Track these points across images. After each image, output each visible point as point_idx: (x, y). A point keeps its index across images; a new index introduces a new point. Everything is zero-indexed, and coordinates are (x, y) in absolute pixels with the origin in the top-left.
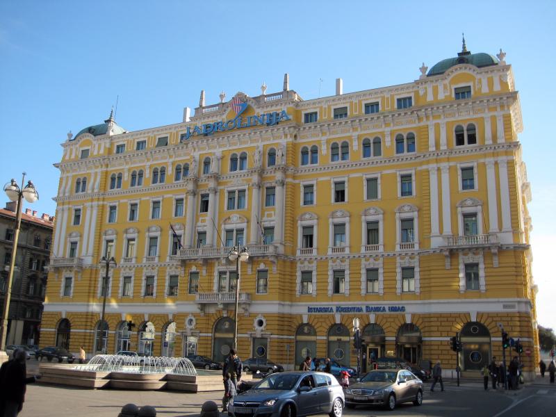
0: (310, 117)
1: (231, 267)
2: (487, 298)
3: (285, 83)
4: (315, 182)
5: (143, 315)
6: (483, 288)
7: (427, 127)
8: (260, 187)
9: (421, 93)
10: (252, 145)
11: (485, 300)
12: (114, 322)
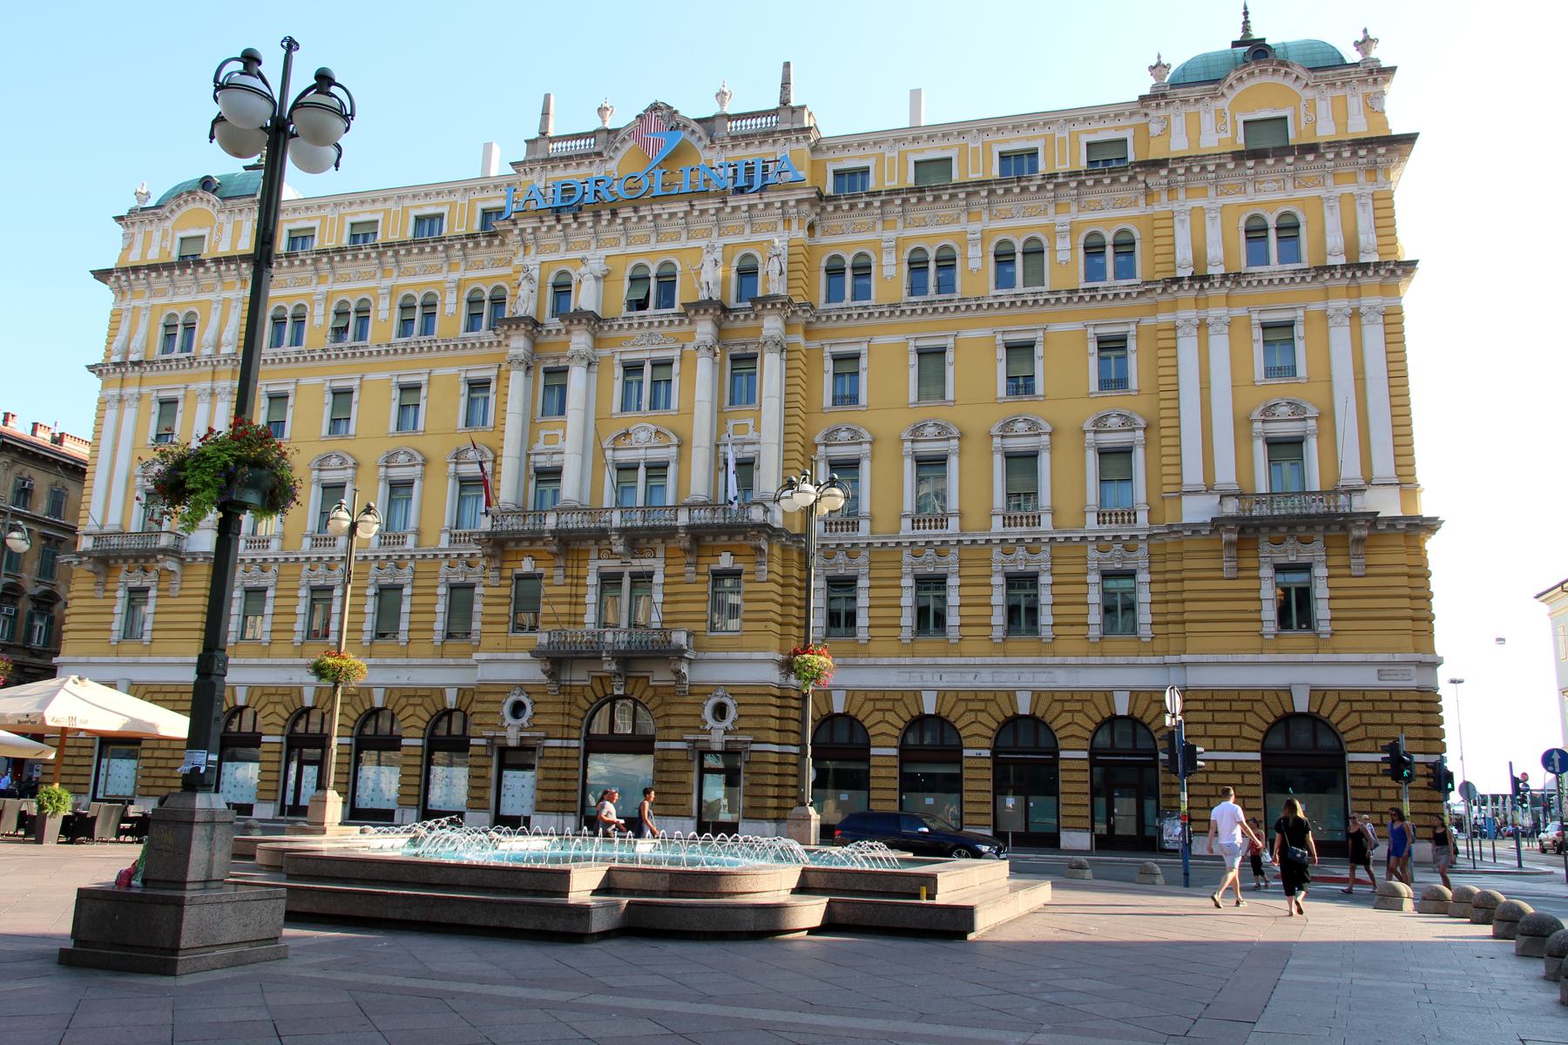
0: (851, 179)
1: (635, 562)
2: (1335, 651)
3: (546, 113)
4: (678, 352)
5: (442, 691)
6: (1145, 631)
7: (1172, 216)
8: (528, 368)
9: (1155, 128)
10: (693, 244)
11: (1334, 658)
12: (280, 709)
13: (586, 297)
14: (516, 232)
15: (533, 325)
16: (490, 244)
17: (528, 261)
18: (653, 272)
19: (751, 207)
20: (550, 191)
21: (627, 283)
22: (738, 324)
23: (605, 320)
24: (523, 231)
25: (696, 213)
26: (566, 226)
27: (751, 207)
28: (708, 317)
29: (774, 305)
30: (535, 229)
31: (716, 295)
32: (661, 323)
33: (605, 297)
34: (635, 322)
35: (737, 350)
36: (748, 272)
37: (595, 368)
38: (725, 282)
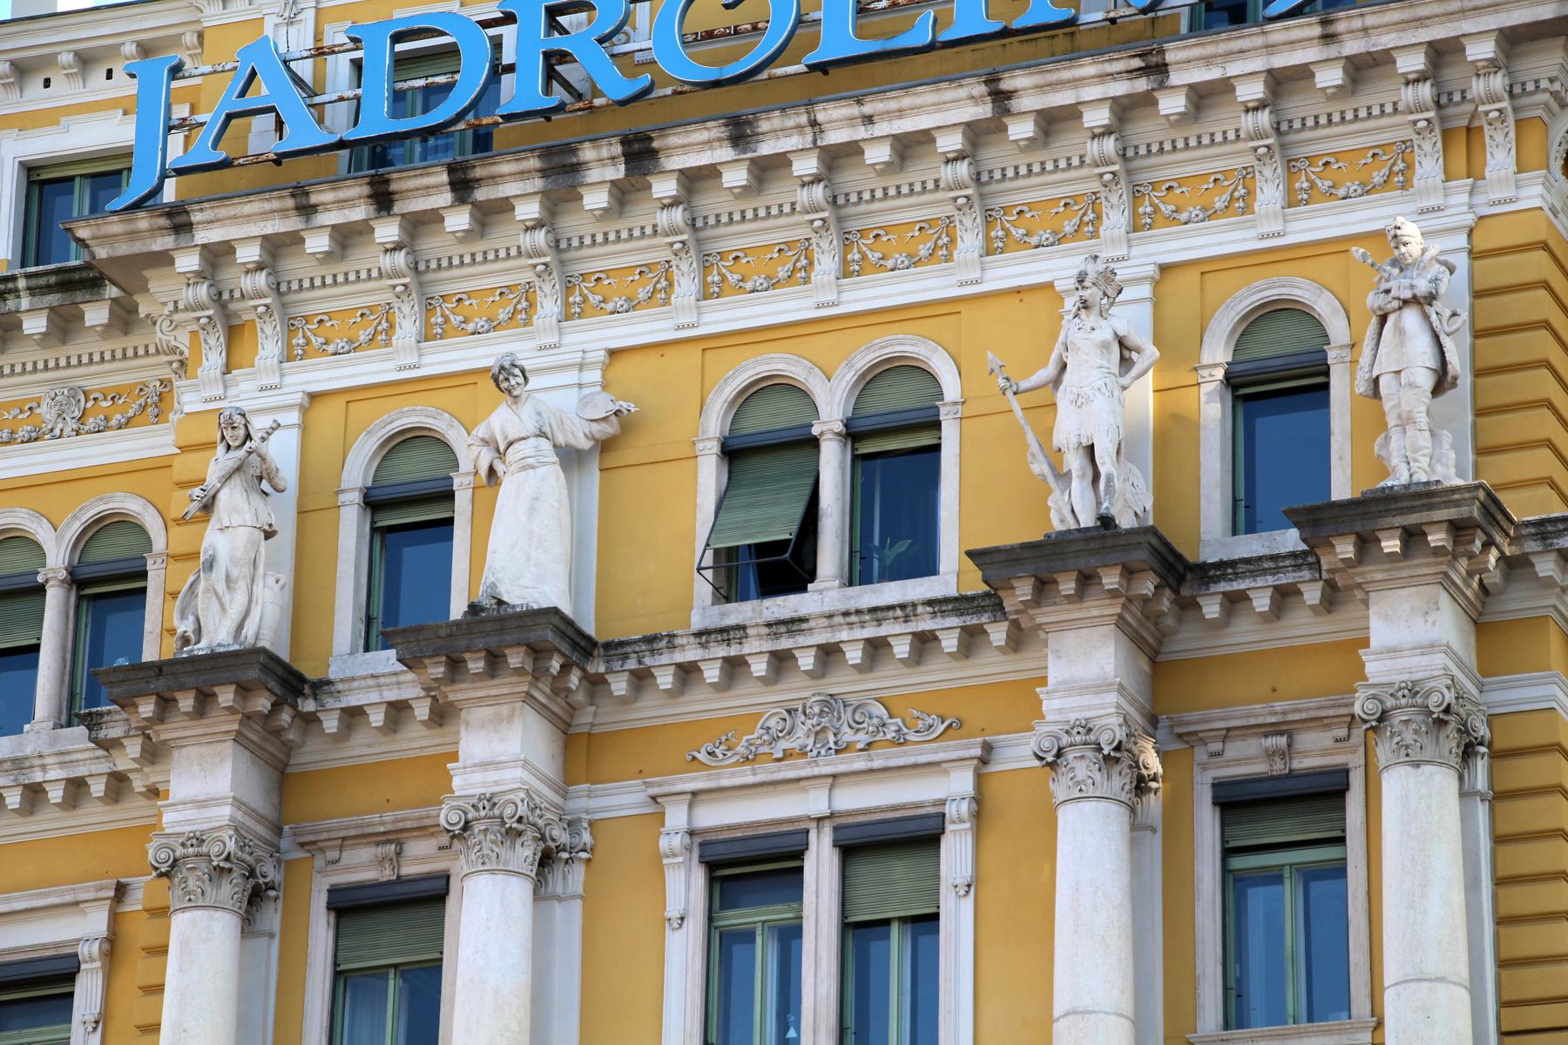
4: (961, 783)
8: (256, 897)
13: (520, 550)
14: (188, 262)
15: (275, 688)
16: (64, 326)
17: (245, 392)
18: (831, 409)
19: (1281, 83)
20: (339, 68)
21: (709, 474)
22: (1245, 634)
23: (615, 649)
24: (218, 255)
25: (1021, 129)
26: (419, 224)
27: (1281, 83)
28: (1099, 608)
29: (1413, 537)
30: (277, 248)
31: (1132, 502)
32: (877, 648)
33: (607, 545)
34: (756, 650)
35: (1248, 760)
36: (1279, 388)
37: (575, 878)
38: (1170, 439)
